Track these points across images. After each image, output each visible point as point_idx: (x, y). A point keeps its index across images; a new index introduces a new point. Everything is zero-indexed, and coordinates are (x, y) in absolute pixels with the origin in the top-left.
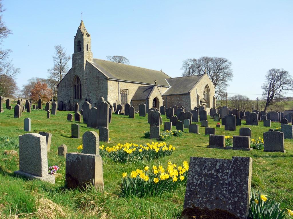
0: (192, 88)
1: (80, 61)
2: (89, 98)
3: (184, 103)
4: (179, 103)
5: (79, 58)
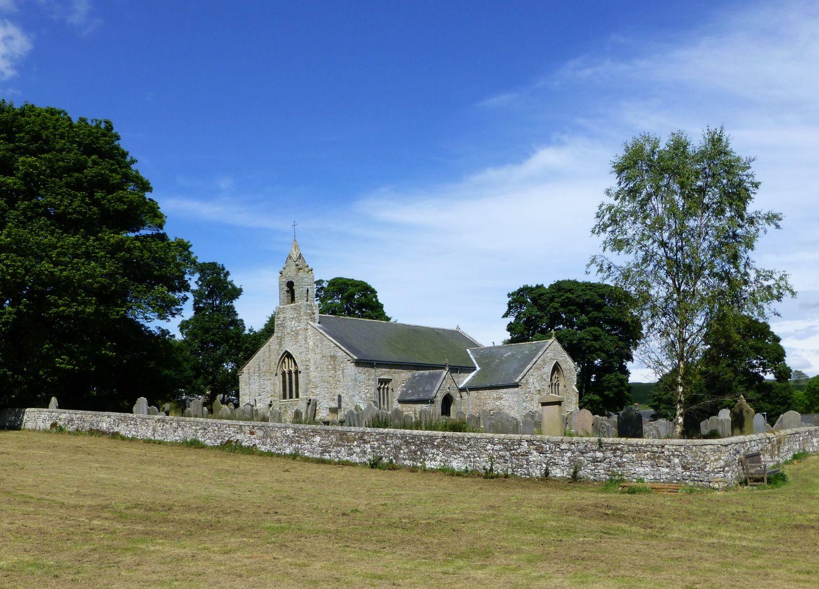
1: (293, 322)
2: (314, 397)
3: (507, 404)
4: (497, 403)
5: (291, 316)
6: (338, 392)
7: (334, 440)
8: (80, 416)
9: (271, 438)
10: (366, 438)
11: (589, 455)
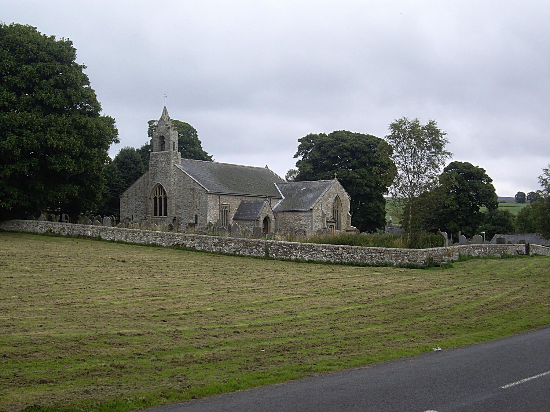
0: (312, 202)
1: (163, 164)
4: (297, 223)
6: (196, 213)
7: (242, 245)
8: (70, 226)
9: (204, 243)
10: (260, 244)
11: (369, 254)
